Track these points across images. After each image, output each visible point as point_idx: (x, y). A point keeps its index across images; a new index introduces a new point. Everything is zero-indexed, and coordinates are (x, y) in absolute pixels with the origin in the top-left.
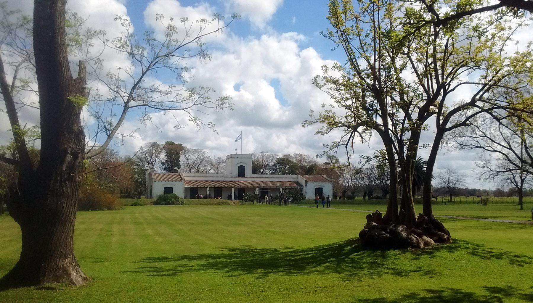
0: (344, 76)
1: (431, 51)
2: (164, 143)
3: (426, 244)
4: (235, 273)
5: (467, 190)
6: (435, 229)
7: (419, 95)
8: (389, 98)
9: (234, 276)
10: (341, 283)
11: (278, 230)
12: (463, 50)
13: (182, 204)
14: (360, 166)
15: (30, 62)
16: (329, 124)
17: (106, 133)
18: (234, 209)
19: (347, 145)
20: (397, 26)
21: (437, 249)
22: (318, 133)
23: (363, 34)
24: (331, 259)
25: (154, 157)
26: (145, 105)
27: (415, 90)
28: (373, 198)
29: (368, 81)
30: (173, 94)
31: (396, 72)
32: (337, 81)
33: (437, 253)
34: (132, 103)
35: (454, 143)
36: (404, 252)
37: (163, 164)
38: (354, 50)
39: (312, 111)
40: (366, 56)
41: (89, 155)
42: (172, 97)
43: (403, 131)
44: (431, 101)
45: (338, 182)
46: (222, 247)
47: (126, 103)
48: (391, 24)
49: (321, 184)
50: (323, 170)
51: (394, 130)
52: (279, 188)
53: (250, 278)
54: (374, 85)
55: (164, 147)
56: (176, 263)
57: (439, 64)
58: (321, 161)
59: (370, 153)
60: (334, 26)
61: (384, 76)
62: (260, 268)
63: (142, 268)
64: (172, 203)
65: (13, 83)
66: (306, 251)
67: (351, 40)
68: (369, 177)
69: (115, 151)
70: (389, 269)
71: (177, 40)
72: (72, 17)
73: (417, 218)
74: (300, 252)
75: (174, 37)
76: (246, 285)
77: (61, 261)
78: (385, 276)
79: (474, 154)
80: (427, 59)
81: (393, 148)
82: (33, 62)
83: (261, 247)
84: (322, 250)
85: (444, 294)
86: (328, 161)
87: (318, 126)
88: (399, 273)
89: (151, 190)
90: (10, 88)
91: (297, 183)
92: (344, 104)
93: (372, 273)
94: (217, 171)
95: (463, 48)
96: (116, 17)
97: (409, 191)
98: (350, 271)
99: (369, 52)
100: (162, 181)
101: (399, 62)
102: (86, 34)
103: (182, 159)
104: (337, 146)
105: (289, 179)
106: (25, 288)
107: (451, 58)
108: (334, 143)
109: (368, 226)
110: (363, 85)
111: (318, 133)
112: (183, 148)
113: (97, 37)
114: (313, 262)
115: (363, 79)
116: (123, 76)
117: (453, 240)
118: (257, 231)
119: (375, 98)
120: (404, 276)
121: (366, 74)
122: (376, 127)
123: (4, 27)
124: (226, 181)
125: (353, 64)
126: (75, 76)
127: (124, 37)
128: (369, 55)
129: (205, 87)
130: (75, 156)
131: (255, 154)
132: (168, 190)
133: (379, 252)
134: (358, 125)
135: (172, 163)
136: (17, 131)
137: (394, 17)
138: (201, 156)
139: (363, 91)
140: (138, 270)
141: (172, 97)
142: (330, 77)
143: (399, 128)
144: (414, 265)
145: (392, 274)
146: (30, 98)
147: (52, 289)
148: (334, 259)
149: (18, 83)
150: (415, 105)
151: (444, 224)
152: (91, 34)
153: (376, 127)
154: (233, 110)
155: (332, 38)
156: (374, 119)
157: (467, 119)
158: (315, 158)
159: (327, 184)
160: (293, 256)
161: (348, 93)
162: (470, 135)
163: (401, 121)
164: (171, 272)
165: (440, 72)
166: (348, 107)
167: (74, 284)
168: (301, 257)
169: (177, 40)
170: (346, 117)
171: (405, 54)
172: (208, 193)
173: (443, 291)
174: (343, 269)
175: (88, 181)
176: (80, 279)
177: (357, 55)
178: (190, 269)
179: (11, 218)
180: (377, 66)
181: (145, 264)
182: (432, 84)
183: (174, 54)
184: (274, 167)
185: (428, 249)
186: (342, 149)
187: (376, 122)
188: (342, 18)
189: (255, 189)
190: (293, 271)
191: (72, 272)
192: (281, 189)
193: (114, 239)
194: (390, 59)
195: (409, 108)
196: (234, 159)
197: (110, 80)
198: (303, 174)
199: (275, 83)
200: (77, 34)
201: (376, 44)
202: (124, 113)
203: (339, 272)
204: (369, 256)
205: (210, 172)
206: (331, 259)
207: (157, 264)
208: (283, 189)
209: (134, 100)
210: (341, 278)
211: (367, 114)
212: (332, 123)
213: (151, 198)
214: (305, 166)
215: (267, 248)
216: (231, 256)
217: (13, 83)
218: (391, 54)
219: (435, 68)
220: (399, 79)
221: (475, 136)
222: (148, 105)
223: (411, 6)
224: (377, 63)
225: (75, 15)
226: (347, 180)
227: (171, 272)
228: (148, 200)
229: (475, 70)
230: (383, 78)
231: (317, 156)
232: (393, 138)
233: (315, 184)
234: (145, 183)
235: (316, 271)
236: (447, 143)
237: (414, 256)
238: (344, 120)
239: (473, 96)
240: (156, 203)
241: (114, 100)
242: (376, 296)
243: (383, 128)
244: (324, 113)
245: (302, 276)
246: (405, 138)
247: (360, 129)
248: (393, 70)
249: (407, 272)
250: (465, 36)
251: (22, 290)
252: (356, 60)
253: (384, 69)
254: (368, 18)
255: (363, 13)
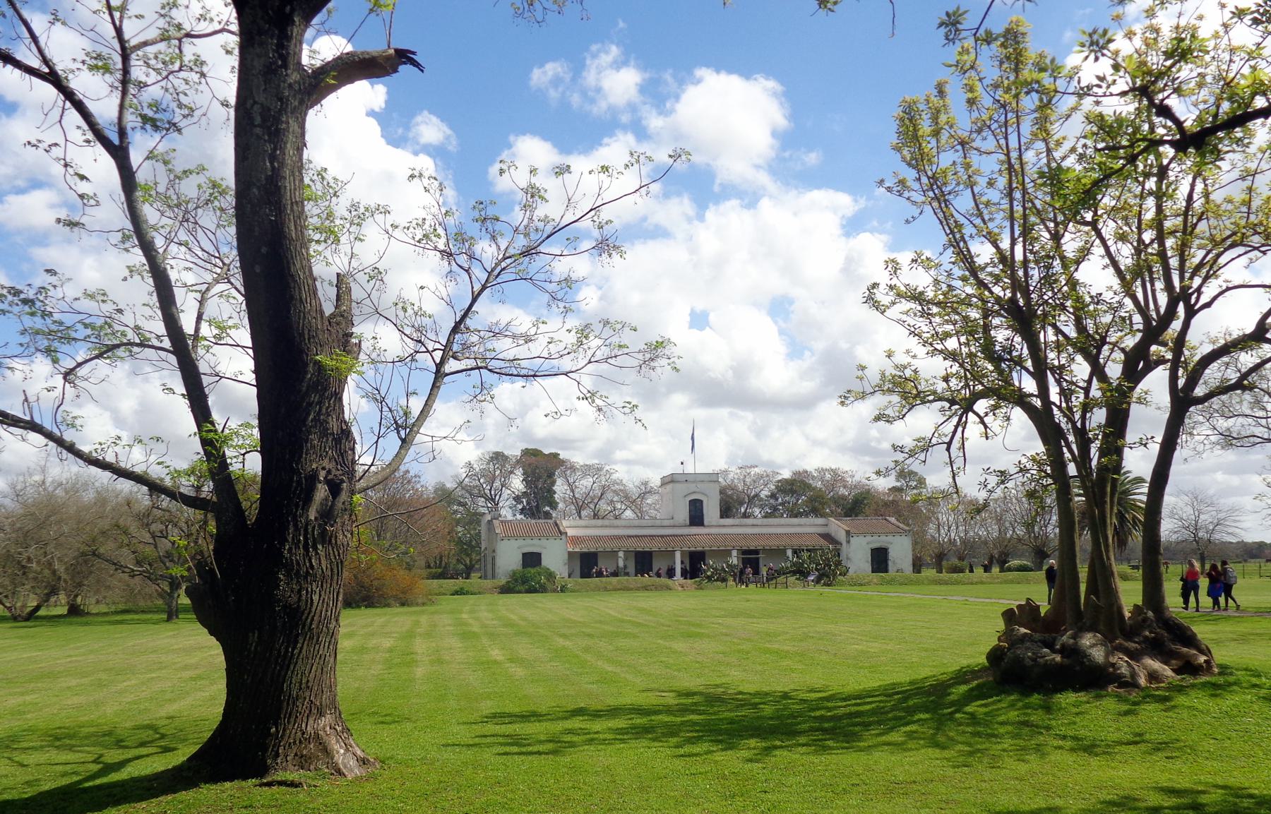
0: (936, 282)
1: (1149, 215)
2: (519, 453)
3: (1153, 676)
4: (696, 749)
5: (1242, 544)
6: (1171, 640)
7: (1123, 319)
8: (1050, 331)
9: (696, 755)
10: (950, 772)
11: (786, 648)
12: (1230, 207)
13: (563, 589)
14: (982, 496)
15: (229, 282)
16: (905, 395)
17: (398, 433)
18: (680, 600)
19: (949, 444)
20: (1063, 158)
21: (1180, 689)
22: (878, 418)
23: (982, 182)
24: (922, 716)
25: (497, 484)
26: (479, 368)
27: (1114, 309)
28: (1009, 570)
29: (997, 290)
30: (543, 340)
31: (1065, 266)
32: (922, 293)
33: (1181, 700)
34: (452, 365)
35: (1209, 432)
36: (1098, 697)
37: (517, 499)
38: (962, 220)
39: (863, 368)
40: (989, 233)
41: (362, 484)
42: (538, 348)
43: (1086, 408)
44: (1153, 333)
45: (924, 533)
46: (662, 688)
47: (439, 366)
48: (1049, 151)
49: (883, 538)
50: (886, 504)
51: (1064, 405)
52: (784, 551)
53: (732, 760)
54: (1013, 300)
55: (518, 462)
56: (561, 726)
57: (1170, 242)
58: (883, 484)
59: (1008, 463)
60: (909, 164)
61: (1036, 278)
62: (752, 736)
63: (485, 736)
64: (542, 589)
65: (197, 329)
66: (858, 697)
67: (951, 197)
68: (999, 520)
69: (412, 473)
70: (1064, 737)
71: (546, 217)
72: (315, 177)
73: (1127, 615)
74: (844, 700)
75: (540, 212)
76: (724, 777)
77: (311, 721)
78: (1056, 756)
79: (1259, 457)
80: (1140, 234)
81: (1065, 450)
82: (238, 281)
83: (750, 688)
84: (897, 693)
85: (1204, 799)
86: (898, 484)
87: (877, 402)
88: (1090, 748)
89: (493, 558)
90: (190, 342)
91: (827, 537)
92: (939, 347)
93: (1023, 749)
94: (640, 513)
95: (1230, 201)
96: (410, 172)
97: (1107, 551)
98: (969, 745)
99: (997, 222)
100: (516, 538)
101: (1071, 244)
102: (347, 214)
103: (560, 488)
104: (925, 449)
105: (809, 527)
106: (236, 783)
107: (1202, 227)
108: (918, 440)
109: (1008, 635)
110: (984, 302)
111: (878, 418)
112: (562, 462)
113: (371, 219)
114: (879, 723)
115: (986, 287)
116: (432, 305)
117: (1221, 666)
118: (739, 651)
119: (1016, 331)
120: (1092, 755)
121: (991, 274)
122: (1021, 399)
123: (169, 206)
124: (662, 536)
125: (959, 253)
126: (328, 309)
127: (429, 217)
128: (996, 230)
129: (612, 321)
130: (335, 488)
131: (726, 472)
132: (532, 559)
133: (1036, 698)
134: (976, 396)
135: (538, 501)
136: (211, 435)
137: (1055, 138)
138: (603, 479)
139: (986, 314)
140: (477, 740)
141: (538, 348)
142: (906, 286)
143: (1078, 399)
144: (1126, 728)
145: (1072, 750)
146: (233, 365)
147: (293, 784)
148: (927, 716)
149: (205, 330)
150: (1115, 344)
151: (1195, 629)
152: (359, 215)
153: (1021, 399)
154: (678, 370)
155: (906, 194)
156: (1017, 384)
157: (1245, 376)
158: (874, 476)
159: (898, 538)
160: (829, 709)
161: (947, 322)
162: (1248, 412)
163: (1082, 384)
164: (550, 746)
165: (1174, 262)
166: (952, 356)
167: (339, 772)
168: (848, 710)
169: (546, 217)
170: (946, 379)
171: (1086, 223)
172: (621, 564)
173: (1204, 792)
174: (952, 739)
175: (358, 542)
176: (352, 763)
177: (968, 230)
178: (592, 740)
179: (199, 625)
180: (1019, 255)
181: (491, 728)
182: (1153, 291)
183: (541, 248)
184: (772, 501)
185: (1158, 689)
186: (939, 453)
187: (1020, 389)
188: (930, 145)
189: (727, 553)
190: (830, 743)
191: (336, 747)
192: (789, 553)
193: (419, 672)
194: (1048, 236)
195: (1099, 352)
196: (677, 485)
197: (401, 313)
198: (840, 515)
199: (779, 308)
200: (330, 216)
201: (1015, 203)
202: (435, 387)
203: (943, 747)
204: (1012, 706)
205: (624, 516)
206: (922, 716)
207: (517, 728)
208: (795, 552)
209: (455, 358)
210: (948, 760)
211: (1000, 372)
212: (908, 391)
213: (493, 577)
214: (843, 498)
215: (766, 689)
216: (684, 710)
217: (197, 329)
218: (1052, 225)
219: (1162, 255)
220: (1073, 283)
221: (1262, 414)
222: (486, 368)
223: (1099, 109)
224: (1019, 249)
225: (321, 173)
226: (947, 528)
227: (550, 746)
228: (488, 583)
229: (1264, 253)
230: (1033, 283)
231: (878, 473)
232: (1063, 425)
233: (869, 538)
234: (479, 545)
235: (889, 744)
236: (1191, 434)
237: (1125, 707)
238: (941, 386)
239: (1259, 317)
240: (506, 590)
241: (413, 360)
242: (1040, 803)
243: (1038, 403)
244: (891, 371)
245: (854, 755)
246: (1094, 425)
247: (982, 406)
248: (1057, 262)
249: (1109, 746)
250: (1236, 174)
251: (229, 788)
252: (965, 242)
253: (1037, 262)
254: (990, 144)
255: (979, 131)
